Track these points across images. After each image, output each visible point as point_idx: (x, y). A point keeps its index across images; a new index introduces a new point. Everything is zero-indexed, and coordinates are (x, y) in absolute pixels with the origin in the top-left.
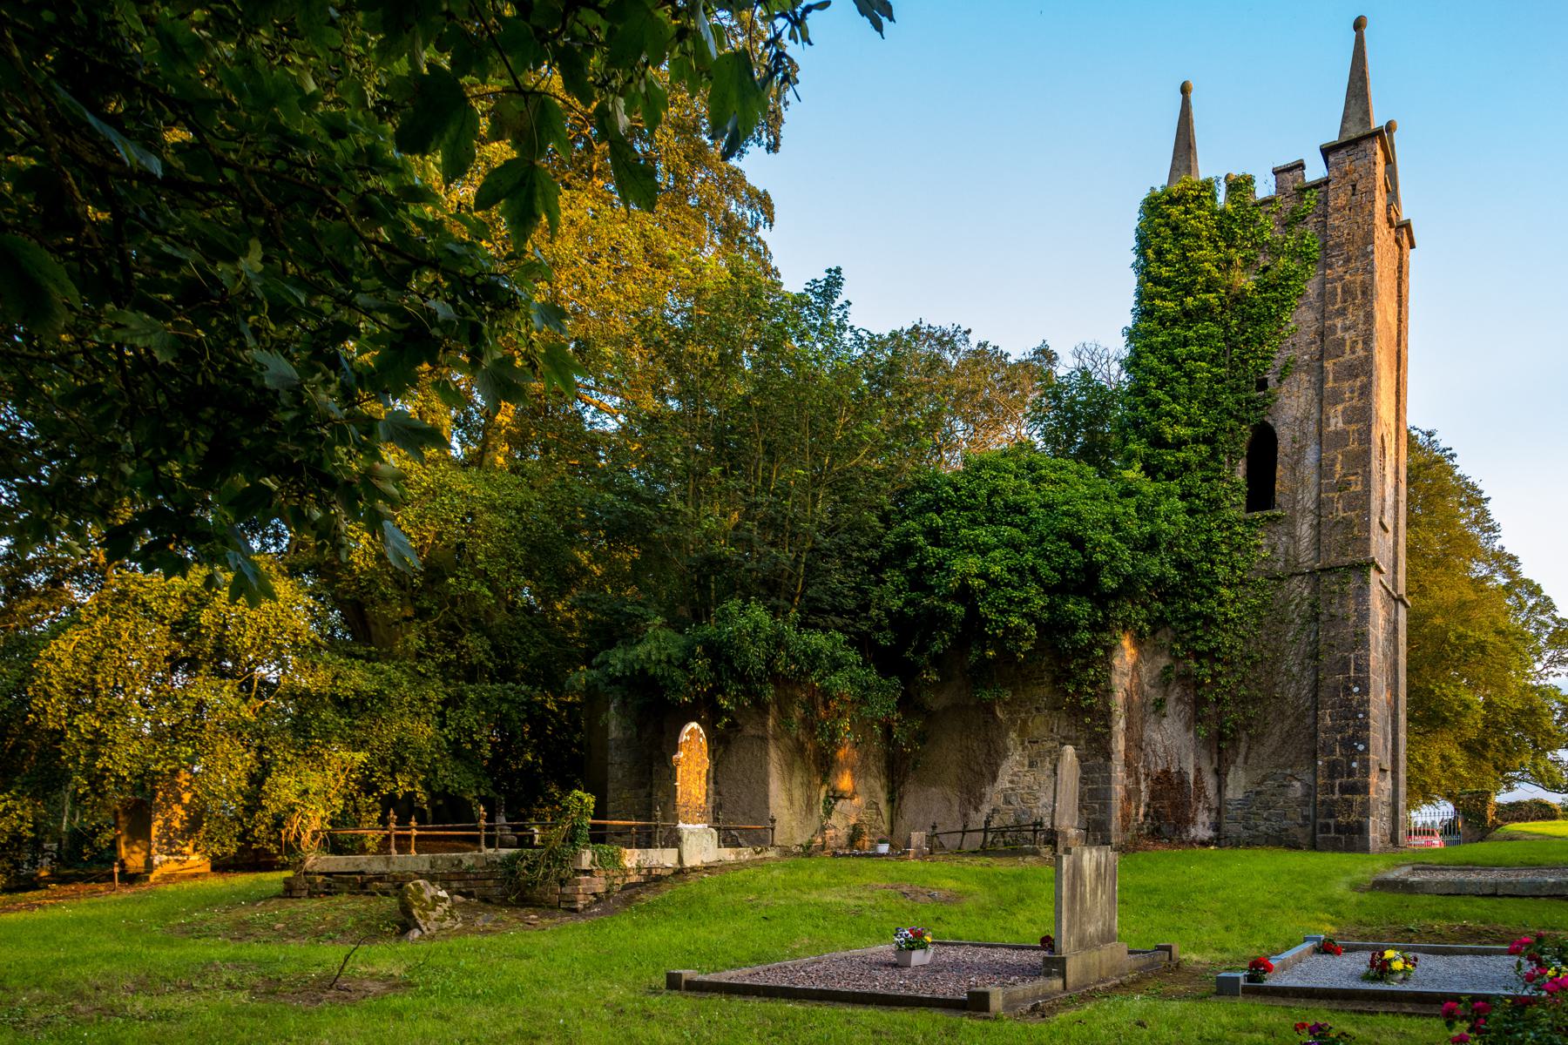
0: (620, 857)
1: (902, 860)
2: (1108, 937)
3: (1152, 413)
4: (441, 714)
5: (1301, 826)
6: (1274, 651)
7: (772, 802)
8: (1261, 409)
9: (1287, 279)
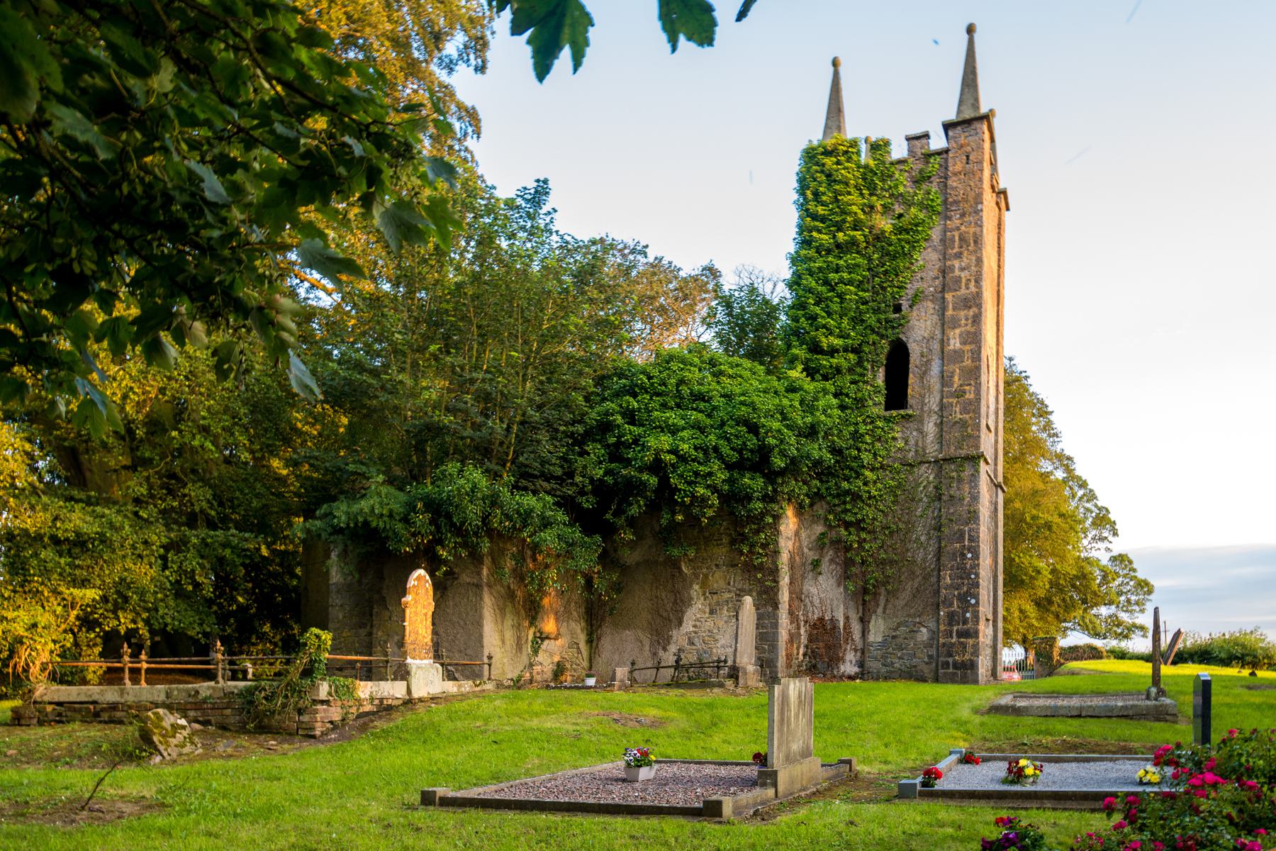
0: (354, 689)
1: (608, 691)
2: (806, 753)
3: (811, 325)
4: (164, 558)
5: (927, 664)
6: (907, 523)
7: (486, 641)
8: (897, 328)
9: (917, 225)
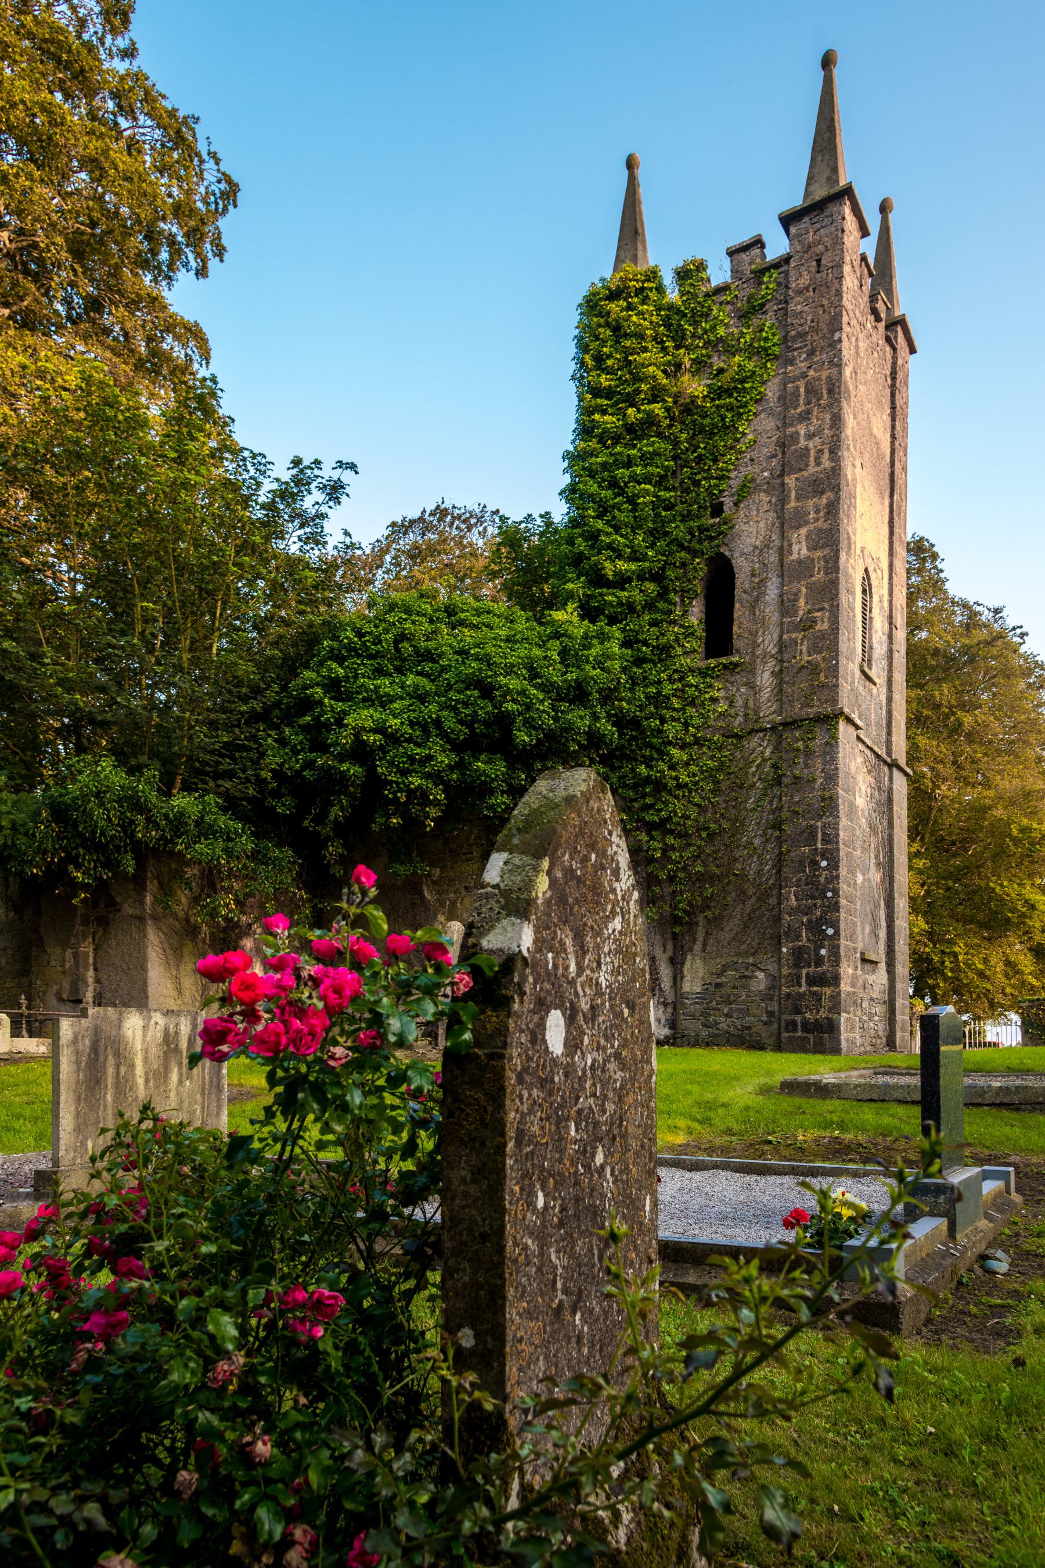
3: (592, 547)
5: (765, 1024)
